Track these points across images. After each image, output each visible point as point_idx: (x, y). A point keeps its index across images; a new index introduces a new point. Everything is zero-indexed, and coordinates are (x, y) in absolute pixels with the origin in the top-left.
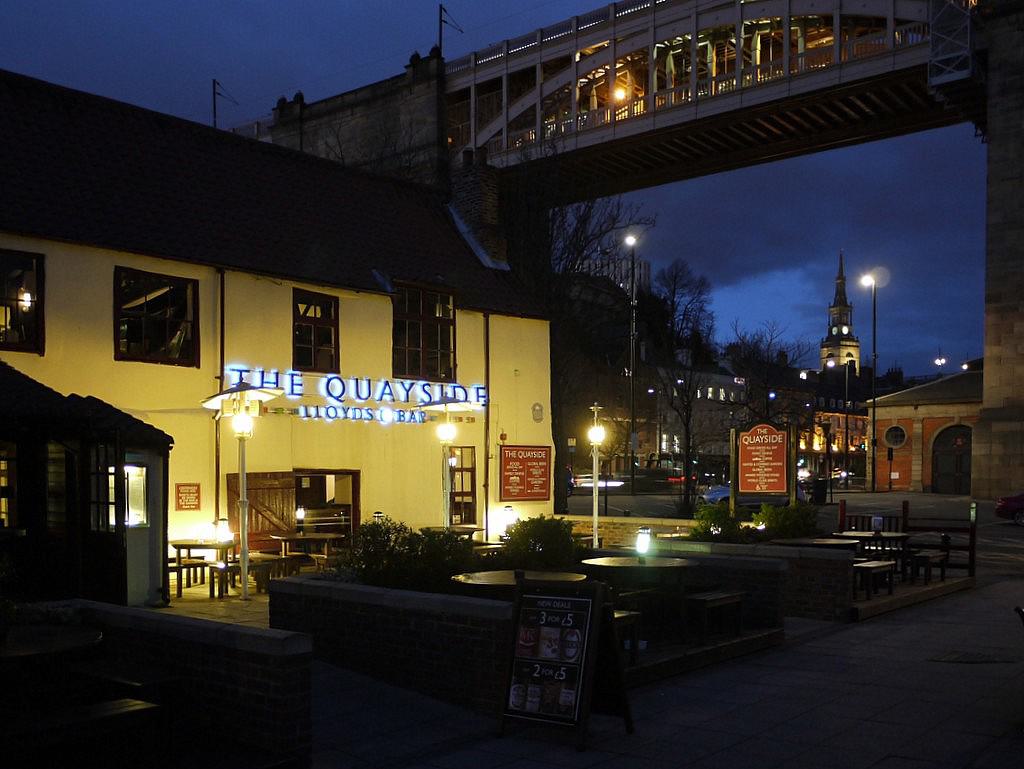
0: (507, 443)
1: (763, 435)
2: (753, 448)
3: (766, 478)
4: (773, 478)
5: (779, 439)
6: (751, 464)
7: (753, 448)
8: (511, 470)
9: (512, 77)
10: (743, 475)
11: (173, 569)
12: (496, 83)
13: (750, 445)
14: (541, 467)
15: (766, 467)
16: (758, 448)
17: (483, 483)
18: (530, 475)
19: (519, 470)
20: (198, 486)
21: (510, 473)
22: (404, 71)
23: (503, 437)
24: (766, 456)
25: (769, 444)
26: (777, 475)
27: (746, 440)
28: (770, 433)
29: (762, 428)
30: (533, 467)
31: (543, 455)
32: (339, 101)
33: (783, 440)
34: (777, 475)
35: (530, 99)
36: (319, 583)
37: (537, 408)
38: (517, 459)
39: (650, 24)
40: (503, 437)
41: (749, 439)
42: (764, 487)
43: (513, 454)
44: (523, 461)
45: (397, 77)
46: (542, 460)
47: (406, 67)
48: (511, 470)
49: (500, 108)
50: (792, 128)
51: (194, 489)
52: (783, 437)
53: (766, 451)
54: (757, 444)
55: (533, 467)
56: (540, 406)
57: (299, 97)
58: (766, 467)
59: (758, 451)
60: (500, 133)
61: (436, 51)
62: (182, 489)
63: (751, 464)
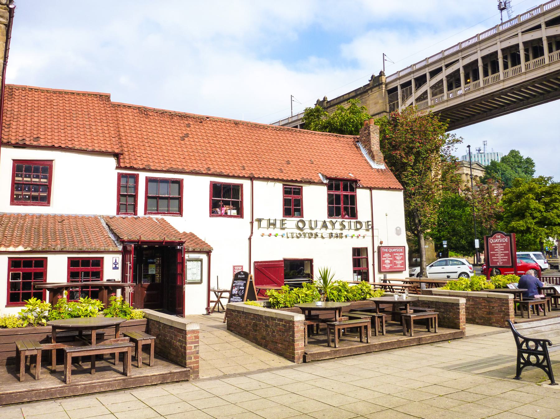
0: (383, 245)
1: (498, 238)
2: (495, 245)
3: (502, 259)
4: (504, 259)
5: (506, 240)
6: (494, 252)
7: (495, 245)
8: (385, 257)
9: (416, 80)
10: (491, 258)
11: (553, 304)
12: (409, 83)
13: (493, 243)
14: (401, 256)
15: (502, 254)
16: (497, 245)
17: (372, 263)
18: (395, 259)
19: (389, 257)
20: (242, 266)
21: (385, 259)
22: (369, 82)
23: (381, 243)
24: (501, 248)
25: (502, 243)
26: (507, 257)
27: (491, 241)
28: (502, 237)
29: (498, 235)
30: (397, 256)
31: (401, 250)
32: (342, 98)
33: (508, 240)
34: (507, 257)
35: (426, 87)
36: (421, 309)
37: (398, 229)
38: (388, 252)
39: (478, 49)
40: (381, 243)
41: (493, 240)
42: (501, 263)
43: (386, 250)
44: (391, 253)
45: (366, 85)
46: (401, 252)
47: (369, 81)
48: (385, 257)
49: (411, 93)
50: (555, 87)
51: (241, 267)
52: (508, 239)
53: (501, 246)
54: (496, 243)
55: (397, 256)
56: (399, 228)
57: (325, 99)
58: (502, 254)
59: (497, 246)
60: (412, 104)
61: (382, 74)
62: (236, 268)
63: (494, 252)
